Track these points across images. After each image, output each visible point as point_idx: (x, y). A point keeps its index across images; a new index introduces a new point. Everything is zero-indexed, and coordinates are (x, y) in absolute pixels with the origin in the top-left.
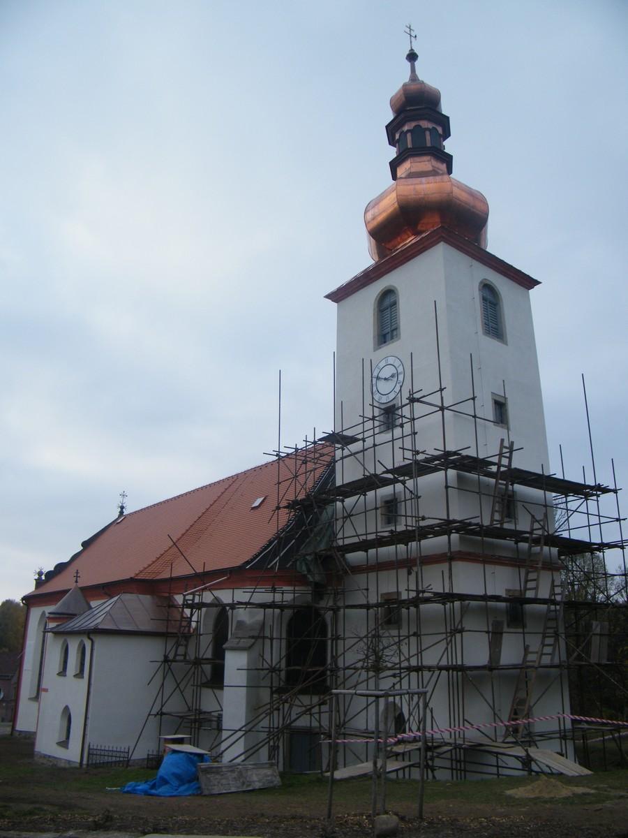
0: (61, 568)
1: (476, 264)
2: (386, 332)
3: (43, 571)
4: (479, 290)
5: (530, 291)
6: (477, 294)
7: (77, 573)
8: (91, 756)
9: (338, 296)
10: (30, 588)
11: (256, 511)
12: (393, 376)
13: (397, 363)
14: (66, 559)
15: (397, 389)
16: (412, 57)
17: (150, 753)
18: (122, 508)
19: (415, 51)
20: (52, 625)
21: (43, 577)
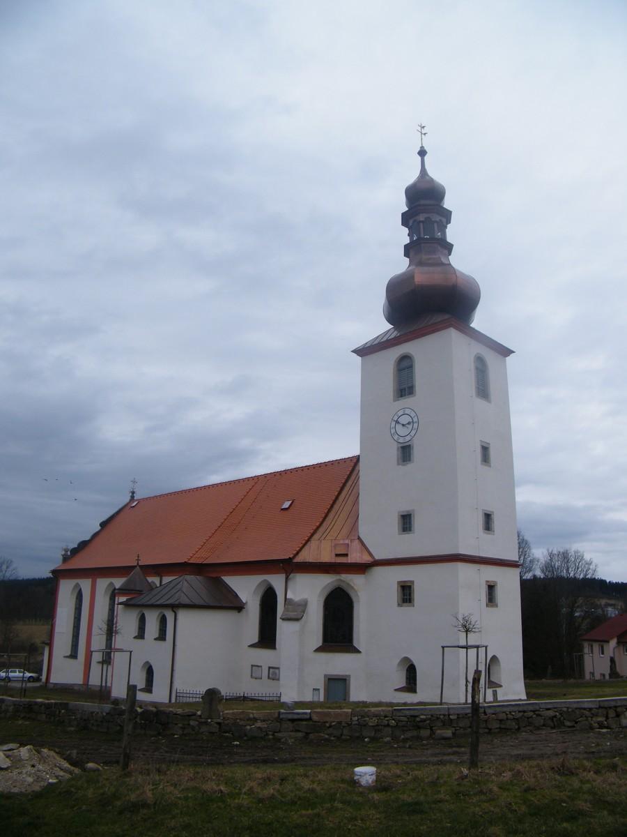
2: (405, 388)
5: (507, 358)
9: (362, 352)
10: (57, 564)
11: (286, 512)
12: (409, 423)
13: (413, 414)
14: (87, 538)
15: (413, 432)
16: (422, 153)
19: (425, 148)
20: (123, 599)
21: (69, 553)
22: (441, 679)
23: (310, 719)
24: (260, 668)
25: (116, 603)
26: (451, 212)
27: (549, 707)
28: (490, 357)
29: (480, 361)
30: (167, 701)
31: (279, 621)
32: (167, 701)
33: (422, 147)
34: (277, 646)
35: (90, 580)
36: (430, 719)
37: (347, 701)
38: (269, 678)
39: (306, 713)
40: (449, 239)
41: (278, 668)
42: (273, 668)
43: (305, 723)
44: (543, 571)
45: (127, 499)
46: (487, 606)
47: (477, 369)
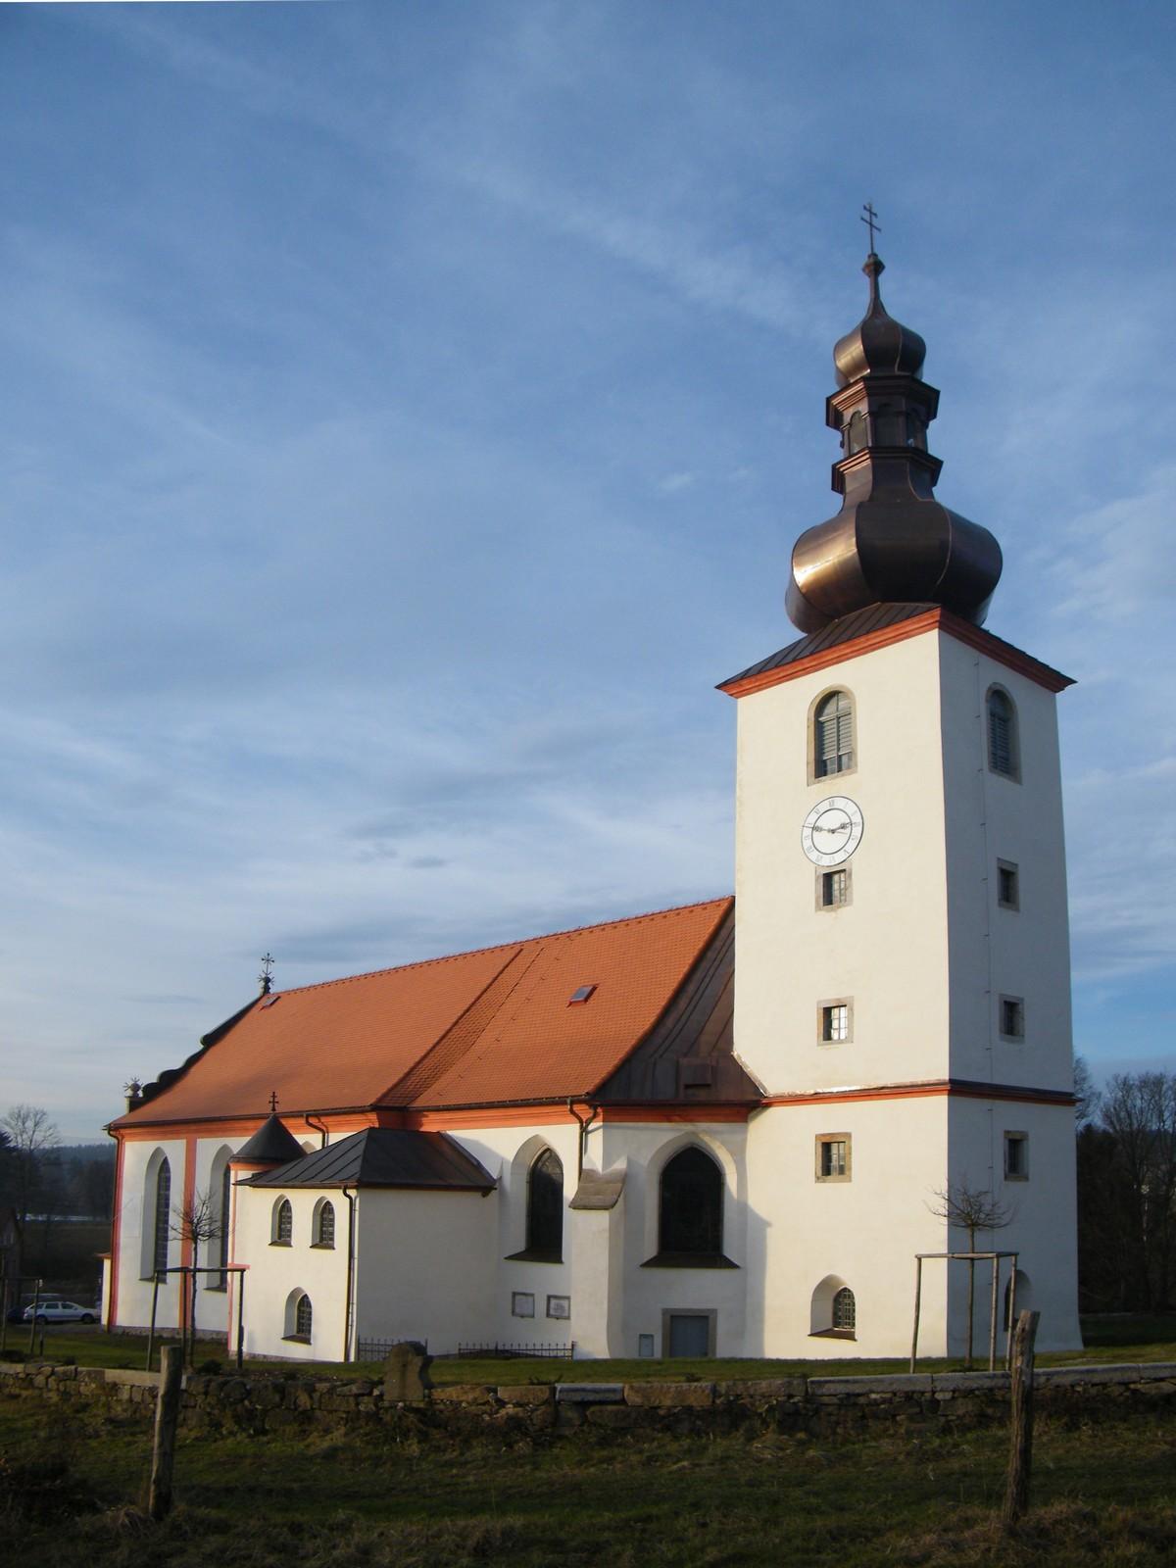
0: (169, 1079)
1: (985, 660)
3: (139, 1083)
4: (987, 701)
5: (1059, 695)
6: (983, 708)
7: (274, 1096)
8: (363, 1353)
12: (843, 827)
15: (850, 847)
16: (875, 268)
17: (462, 1347)
18: (267, 980)
21: (141, 1094)
22: (914, 1317)
23: (623, 1401)
24: (530, 1299)
25: (232, 1181)
26: (937, 393)
27: (1162, 1374)
28: (1018, 688)
29: (999, 698)
30: (342, 1360)
31: (568, 1213)
32: (340, 1358)
33: (874, 255)
34: (563, 1259)
35: (184, 1141)
36: (890, 1401)
37: (710, 1355)
38: (548, 1315)
39: (614, 1391)
40: (933, 450)
41: (568, 1298)
42: (556, 1297)
43: (610, 1408)
44: (1107, 1116)
45: (258, 992)
46: (1006, 1178)
47: (993, 715)
